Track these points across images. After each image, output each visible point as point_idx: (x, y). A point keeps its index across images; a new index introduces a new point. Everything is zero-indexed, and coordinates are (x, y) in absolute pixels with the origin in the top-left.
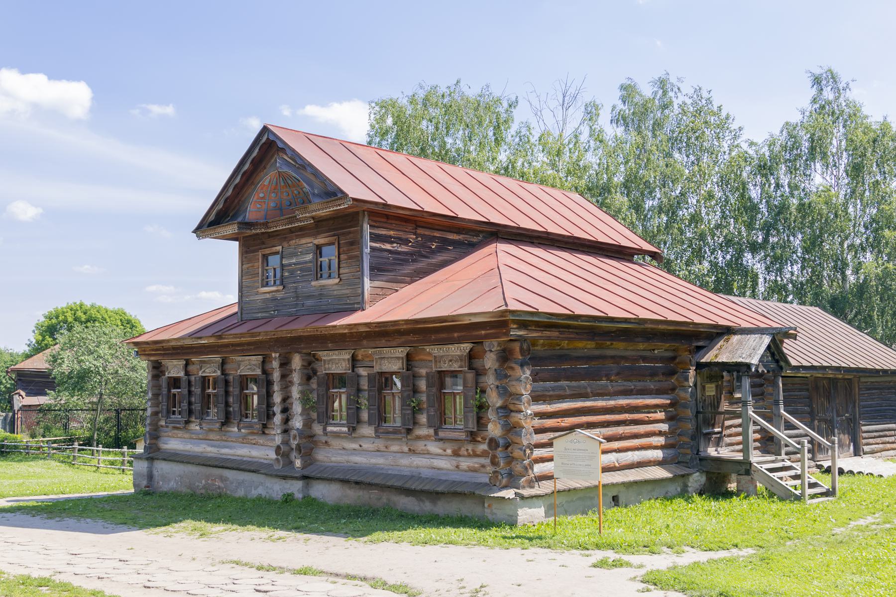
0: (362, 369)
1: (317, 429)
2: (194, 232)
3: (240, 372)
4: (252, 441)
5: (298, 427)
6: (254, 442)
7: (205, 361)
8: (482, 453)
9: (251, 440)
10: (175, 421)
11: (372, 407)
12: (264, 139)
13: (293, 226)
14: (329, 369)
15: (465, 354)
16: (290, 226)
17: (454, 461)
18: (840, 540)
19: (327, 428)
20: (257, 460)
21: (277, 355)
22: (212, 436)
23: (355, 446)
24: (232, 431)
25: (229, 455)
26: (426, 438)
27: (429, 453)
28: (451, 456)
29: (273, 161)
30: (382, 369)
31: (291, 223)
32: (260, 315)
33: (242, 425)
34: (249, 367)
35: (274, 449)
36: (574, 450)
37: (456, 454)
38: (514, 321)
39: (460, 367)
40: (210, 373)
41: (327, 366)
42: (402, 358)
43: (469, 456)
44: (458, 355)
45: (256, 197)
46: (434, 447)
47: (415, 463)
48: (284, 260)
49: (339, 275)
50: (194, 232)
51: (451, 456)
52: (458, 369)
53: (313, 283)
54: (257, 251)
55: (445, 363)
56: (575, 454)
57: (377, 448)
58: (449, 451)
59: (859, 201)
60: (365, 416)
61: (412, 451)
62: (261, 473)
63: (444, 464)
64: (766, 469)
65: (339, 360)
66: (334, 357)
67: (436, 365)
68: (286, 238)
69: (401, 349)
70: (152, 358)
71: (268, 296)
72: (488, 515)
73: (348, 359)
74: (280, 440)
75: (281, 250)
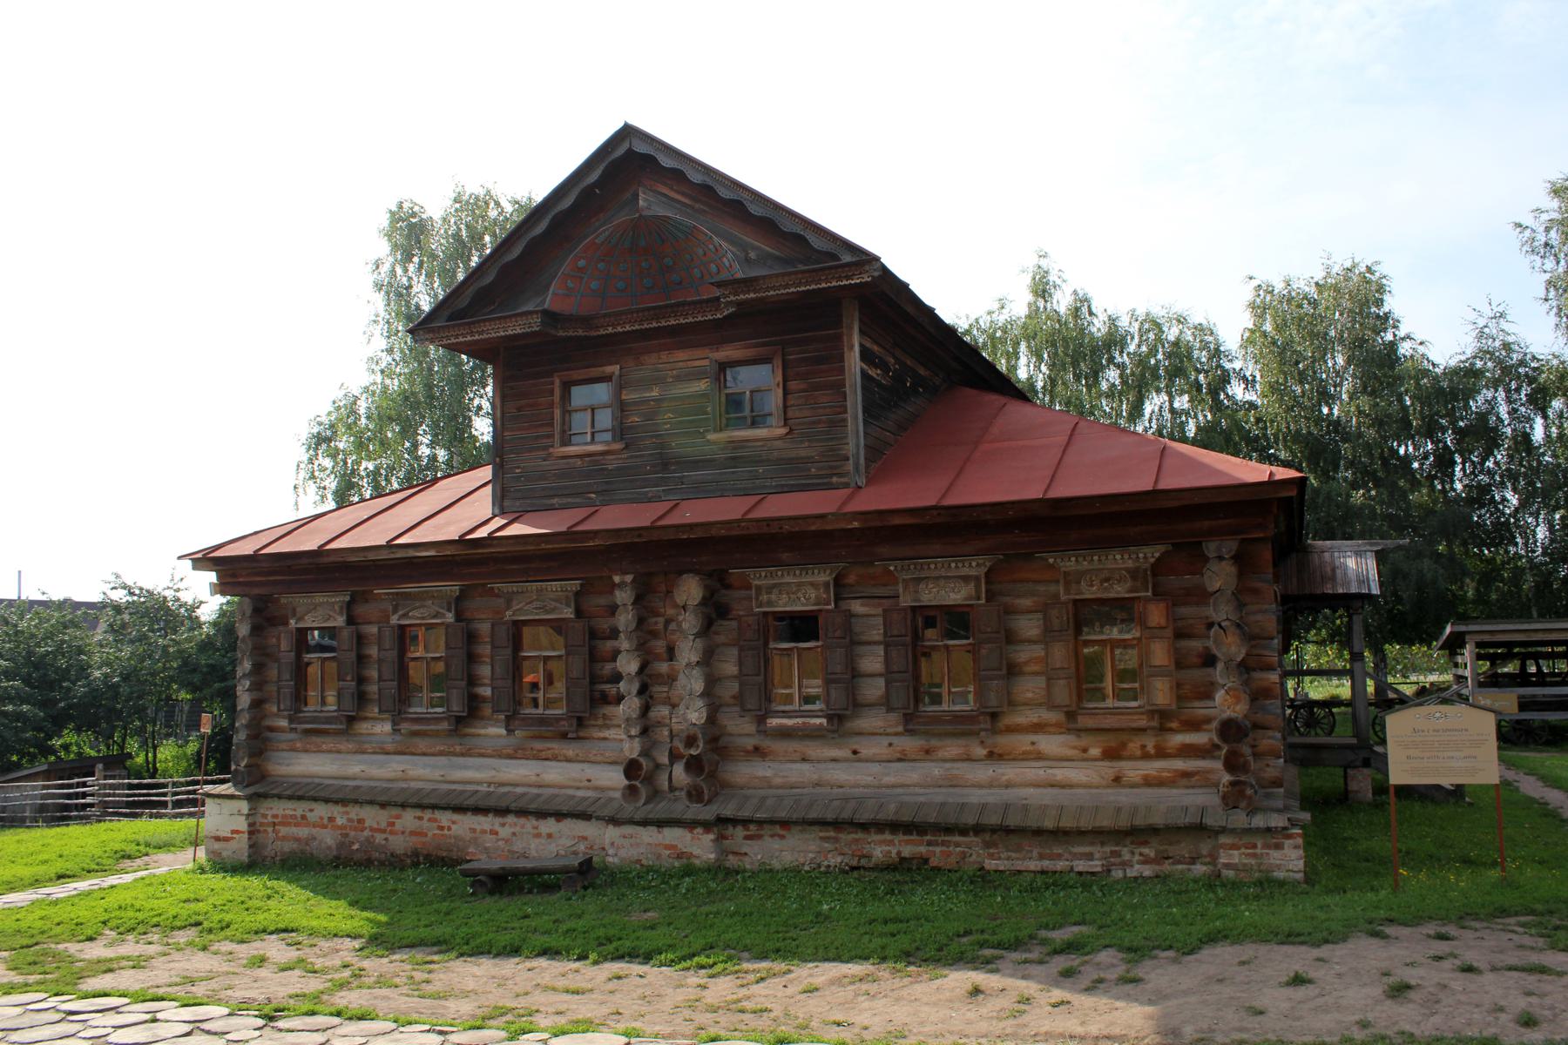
0: (859, 601)
1: (739, 727)
3: (513, 615)
7: (410, 593)
8: (1178, 750)
12: (620, 151)
13: (664, 324)
14: (770, 603)
15: (1147, 565)
16: (655, 325)
17: (1108, 769)
18: (341, 1006)
21: (629, 578)
22: (422, 744)
24: (479, 735)
27: (1039, 757)
29: (628, 195)
30: (919, 601)
31: (658, 319)
35: (621, 769)
36: (1434, 731)
37: (1111, 754)
39: (1131, 591)
40: (423, 618)
41: (765, 597)
42: (977, 579)
43: (1146, 756)
44: (1127, 570)
47: (1005, 778)
48: (624, 392)
49: (785, 420)
52: (1127, 596)
53: (712, 437)
55: (1092, 586)
56: (1454, 738)
57: (898, 755)
58: (1095, 752)
59: (1108, 410)
60: (874, 689)
61: (993, 756)
65: (800, 585)
67: (1067, 591)
69: (981, 560)
70: (256, 591)
73: (827, 585)
75: (617, 373)
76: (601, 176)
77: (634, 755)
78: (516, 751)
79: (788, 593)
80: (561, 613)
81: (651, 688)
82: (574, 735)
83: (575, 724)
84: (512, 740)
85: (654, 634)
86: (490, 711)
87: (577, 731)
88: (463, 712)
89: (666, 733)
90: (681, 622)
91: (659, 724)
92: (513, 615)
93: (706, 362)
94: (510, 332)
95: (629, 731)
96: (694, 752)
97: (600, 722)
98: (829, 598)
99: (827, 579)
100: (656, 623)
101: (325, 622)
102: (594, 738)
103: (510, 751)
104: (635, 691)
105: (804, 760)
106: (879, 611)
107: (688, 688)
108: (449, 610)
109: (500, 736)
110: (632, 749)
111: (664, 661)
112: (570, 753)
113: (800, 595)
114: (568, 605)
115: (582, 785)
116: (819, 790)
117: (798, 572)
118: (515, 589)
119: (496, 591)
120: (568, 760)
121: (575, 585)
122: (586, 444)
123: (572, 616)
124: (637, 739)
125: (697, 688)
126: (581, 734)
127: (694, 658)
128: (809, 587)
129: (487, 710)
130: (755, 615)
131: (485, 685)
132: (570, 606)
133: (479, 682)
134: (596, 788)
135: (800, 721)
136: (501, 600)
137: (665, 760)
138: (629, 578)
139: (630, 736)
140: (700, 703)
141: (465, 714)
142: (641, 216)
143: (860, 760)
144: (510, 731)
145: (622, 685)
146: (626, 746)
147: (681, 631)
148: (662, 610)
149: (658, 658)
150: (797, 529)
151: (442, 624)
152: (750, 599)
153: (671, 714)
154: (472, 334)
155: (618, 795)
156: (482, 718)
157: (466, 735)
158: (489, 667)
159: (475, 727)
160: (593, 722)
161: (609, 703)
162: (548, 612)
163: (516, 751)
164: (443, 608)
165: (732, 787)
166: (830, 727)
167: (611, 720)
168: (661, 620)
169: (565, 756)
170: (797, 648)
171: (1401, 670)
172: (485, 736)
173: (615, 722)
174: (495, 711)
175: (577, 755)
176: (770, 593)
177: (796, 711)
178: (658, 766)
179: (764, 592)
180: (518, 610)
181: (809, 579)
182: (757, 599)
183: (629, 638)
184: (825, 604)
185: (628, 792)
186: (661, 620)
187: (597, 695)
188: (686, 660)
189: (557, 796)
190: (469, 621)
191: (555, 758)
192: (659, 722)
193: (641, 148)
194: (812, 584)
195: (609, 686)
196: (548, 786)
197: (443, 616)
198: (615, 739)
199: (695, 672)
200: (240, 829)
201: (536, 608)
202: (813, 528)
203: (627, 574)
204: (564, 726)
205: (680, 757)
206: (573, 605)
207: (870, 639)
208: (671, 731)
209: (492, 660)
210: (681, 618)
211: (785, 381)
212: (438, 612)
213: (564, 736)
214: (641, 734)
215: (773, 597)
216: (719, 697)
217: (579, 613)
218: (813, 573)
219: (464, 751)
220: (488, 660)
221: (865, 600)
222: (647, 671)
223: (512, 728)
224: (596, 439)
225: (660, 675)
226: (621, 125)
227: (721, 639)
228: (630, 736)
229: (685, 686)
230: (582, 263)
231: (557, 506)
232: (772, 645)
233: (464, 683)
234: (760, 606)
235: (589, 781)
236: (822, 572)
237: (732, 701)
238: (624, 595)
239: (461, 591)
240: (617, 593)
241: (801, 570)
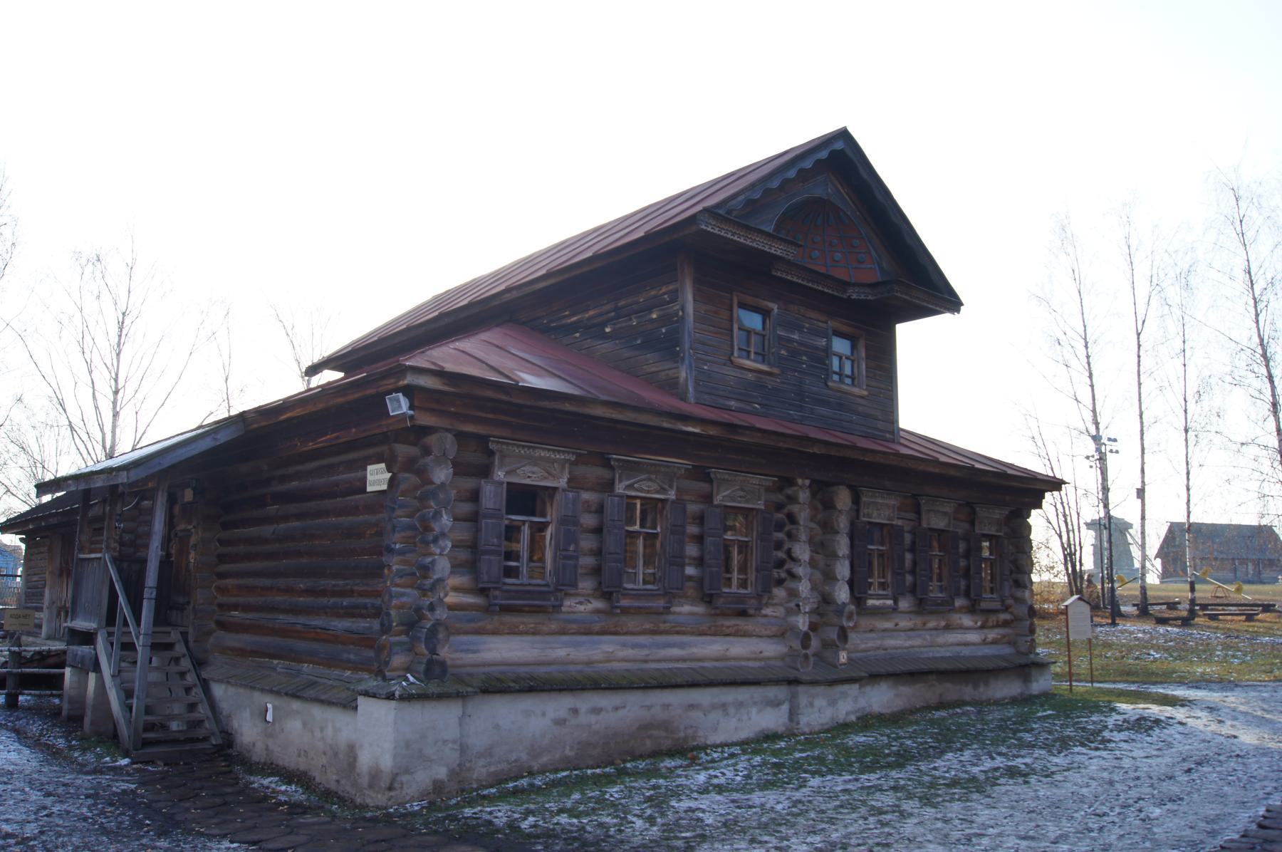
5: (844, 600)
9: (728, 627)
10: (529, 592)
11: (923, 572)
14: (869, 516)
21: (807, 482)
23: (888, 625)
26: (960, 610)
28: (910, 612)
32: (732, 403)
38: (746, 560)
40: (648, 492)
46: (967, 621)
51: (910, 612)
61: (948, 628)
63: (973, 637)
64: (735, 217)
66: (880, 500)
71: (750, 376)
72: (348, 788)
74: (807, 624)
78: (710, 628)
94: (772, 251)
101: (542, 480)
105: (871, 631)
154: (746, 238)
171: (391, 584)
172: (680, 614)
181: (887, 501)
231: (733, 408)
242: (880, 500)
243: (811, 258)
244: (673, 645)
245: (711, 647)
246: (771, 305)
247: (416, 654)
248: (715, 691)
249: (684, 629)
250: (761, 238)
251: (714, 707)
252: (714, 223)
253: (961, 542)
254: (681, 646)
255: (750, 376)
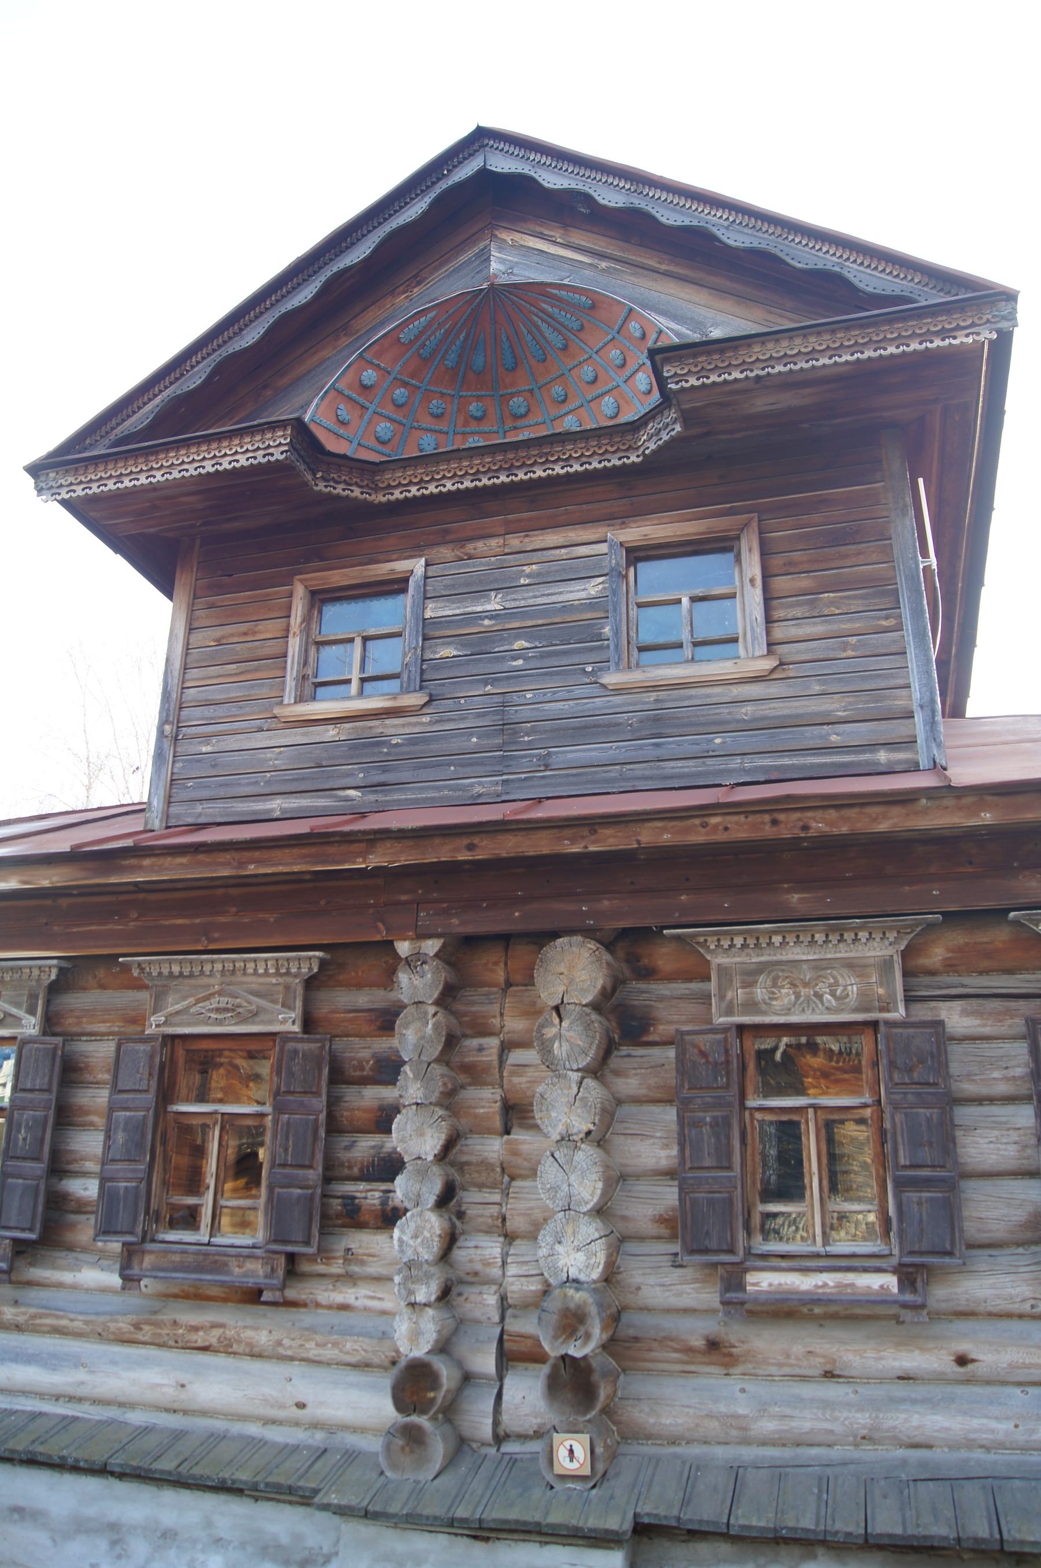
0: (958, 1005)
2: (35, 470)
3: (165, 1023)
4: (193, 1337)
6: (213, 1337)
7: (892, 674)
9: (196, 1329)
14: (751, 1006)
19: (751, 1278)
20: (219, 1425)
21: (431, 946)
25: (25, 1393)
33: (148, 1260)
34: (223, 1001)
35: (386, 1381)
45: (350, 377)
49: (770, 645)
50: (35, 470)
54: (287, 580)
62: (325, 1507)
65: (820, 967)
68: (447, 532)
71: (331, 733)
73: (886, 965)
76: (425, 214)
77: (420, 1351)
78: (137, 1327)
79: (793, 985)
80: (270, 1022)
81: (461, 1194)
82: (276, 1296)
83: (281, 1272)
84: (132, 1300)
85: (474, 1074)
86: (91, 1232)
87: (283, 1288)
88: (31, 1230)
89: (492, 1300)
90: (552, 1040)
91: (476, 1279)
92: (165, 1023)
93: (603, 548)
95: (411, 1292)
96: (576, 1350)
97: (336, 1268)
98: (893, 995)
99: (890, 951)
100: (481, 1049)
102: (318, 1305)
103: (123, 1325)
104: (431, 1200)
106: (1017, 1024)
107: (561, 1194)
108: (32, 1011)
109: (104, 1290)
110: (415, 1335)
111: (495, 1133)
112: (263, 1338)
113: (822, 988)
114: (287, 1005)
115: (281, 1414)
116: (868, 1453)
117: (819, 937)
118: (176, 969)
119: (135, 973)
120: (256, 1354)
121: (309, 962)
122: (350, 698)
123: (296, 1028)
124: (430, 1312)
125: (586, 1196)
126: (291, 1294)
127: (581, 1123)
128: (845, 971)
129: (85, 1229)
130: (714, 1031)
131: (85, 1174)
132: (292, 1008)
133: (89, 1078)
134: (315, 1425)
135: (830, 1279)
136: (144, 996)
137: (486, 1362)
138: (431, 946)
139: (412, 1305)
140: (590, 1229)
141: (33, 1236)
142: (492, 285)
143: (969, 1381)
144: (129, 1280)
145: (401, 1187)
146: (402, 1327)
147: (550, 1063)
148: (496, 1022)
149: (483, 1130)
150: (845, 829)
151: (13, 1039)
152: (705, 998)
153: (505, 1256)
155: (374, 1444)
156: (70, 1248)
157: (30, 1284)
158: (101, 1137)
159: (55, 1268)
160: (321, 1268)
161: (360, 1225)
162: (244, 1021)
163: (137, 1327)
164: (18, 1005)
165: (649, 1437)
166: (908, 1297)
167: (362, 1263)
168: (494, 1042)
169: (250, 1345)
170: (816, 1108)
172: (74, 1287)
173: (372, 1269)
174: (106, 1230)
175: (279, 1343)
176: (752, 984)
177: (817, 1256)
178: (467, 1378)
179: (737, 981)
180: (178, 1013)
181: (844, 952)
182: (722, 997)
183: (423, 1076)
184: (882, 1010)
185: (400, 1442)
186: (494, 1042)
187: (336, 1205)
188: (561, 1128)
189: (223, 1437)
190: (70, 1037)
191: (226, 1348)
192: (476, 1274)
193: (502, 164)
194: (851, 965)
195: (362, 1186)
196: (204, 1413)
197: (17, 1021)
198: (366, 1309)
199: (580, 1156)
200: (508, 1224)
201: (218, 1010)
202: (883, 827)
203: (429, 936)
204: (255, 1272)
205: (536, 1357)
206: (299, 1004)
207: (984, 1091)
208: (503, 1298)
209: (109, 1117)
210: (550, 1032)
211: (766, 576)
212: (7, 1015)
213: (253, 1296)
214: (439, 1299)
215: (760, 993)
216: (624, 1218)
217: (309, 1023)
218: (856, 940)
219: (21, 1319)
220: (99, 1121)
221: (974, 1003)
222: (451, 1156)
223: (136, 1271)
224: (366, 693)
225: (485, 1165)
226: (472, 128)
227: (630, 1085)
228: (412, 1305)
229: (555, 1189)
230: (369, 376)
232: (752, 1102)
233: (39, 1167)
234: (729, 1011)
235: (301, 1406)
236: (877, 936)
237: (652, 1229)
238: (417, 981)
239: (61, 970)
240: (403, 977)
241: (834, 929)
242: (796, 953)
243: (516, 417)
244: (30, 1359)
245: (132, 1375)
246: (401, 566)
247: (544, 1311)
248: (92, 1484)
249: (64, 1322)
250: (126, 468)
251: (81, 1527)
252: (71, 479)
253: (43, 1113)
254: (50, 1361)
255: (331, 733)
